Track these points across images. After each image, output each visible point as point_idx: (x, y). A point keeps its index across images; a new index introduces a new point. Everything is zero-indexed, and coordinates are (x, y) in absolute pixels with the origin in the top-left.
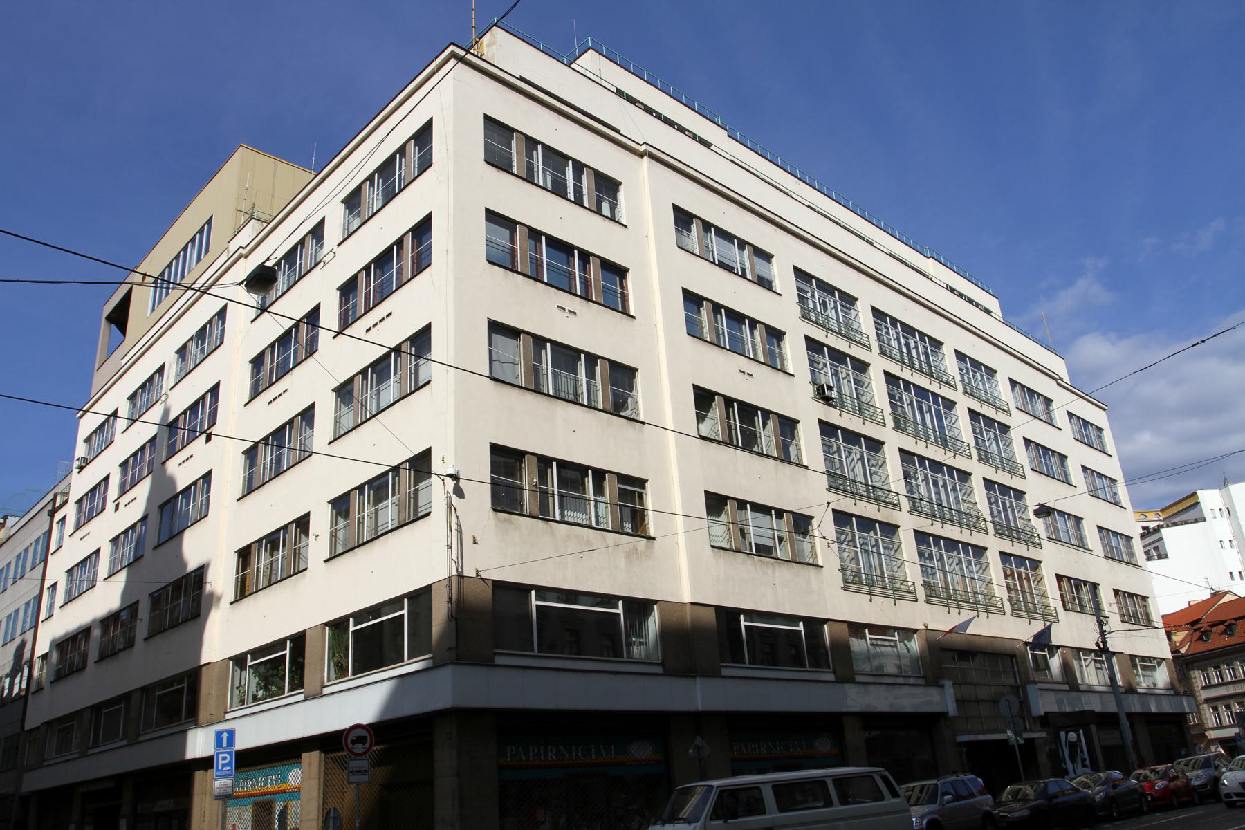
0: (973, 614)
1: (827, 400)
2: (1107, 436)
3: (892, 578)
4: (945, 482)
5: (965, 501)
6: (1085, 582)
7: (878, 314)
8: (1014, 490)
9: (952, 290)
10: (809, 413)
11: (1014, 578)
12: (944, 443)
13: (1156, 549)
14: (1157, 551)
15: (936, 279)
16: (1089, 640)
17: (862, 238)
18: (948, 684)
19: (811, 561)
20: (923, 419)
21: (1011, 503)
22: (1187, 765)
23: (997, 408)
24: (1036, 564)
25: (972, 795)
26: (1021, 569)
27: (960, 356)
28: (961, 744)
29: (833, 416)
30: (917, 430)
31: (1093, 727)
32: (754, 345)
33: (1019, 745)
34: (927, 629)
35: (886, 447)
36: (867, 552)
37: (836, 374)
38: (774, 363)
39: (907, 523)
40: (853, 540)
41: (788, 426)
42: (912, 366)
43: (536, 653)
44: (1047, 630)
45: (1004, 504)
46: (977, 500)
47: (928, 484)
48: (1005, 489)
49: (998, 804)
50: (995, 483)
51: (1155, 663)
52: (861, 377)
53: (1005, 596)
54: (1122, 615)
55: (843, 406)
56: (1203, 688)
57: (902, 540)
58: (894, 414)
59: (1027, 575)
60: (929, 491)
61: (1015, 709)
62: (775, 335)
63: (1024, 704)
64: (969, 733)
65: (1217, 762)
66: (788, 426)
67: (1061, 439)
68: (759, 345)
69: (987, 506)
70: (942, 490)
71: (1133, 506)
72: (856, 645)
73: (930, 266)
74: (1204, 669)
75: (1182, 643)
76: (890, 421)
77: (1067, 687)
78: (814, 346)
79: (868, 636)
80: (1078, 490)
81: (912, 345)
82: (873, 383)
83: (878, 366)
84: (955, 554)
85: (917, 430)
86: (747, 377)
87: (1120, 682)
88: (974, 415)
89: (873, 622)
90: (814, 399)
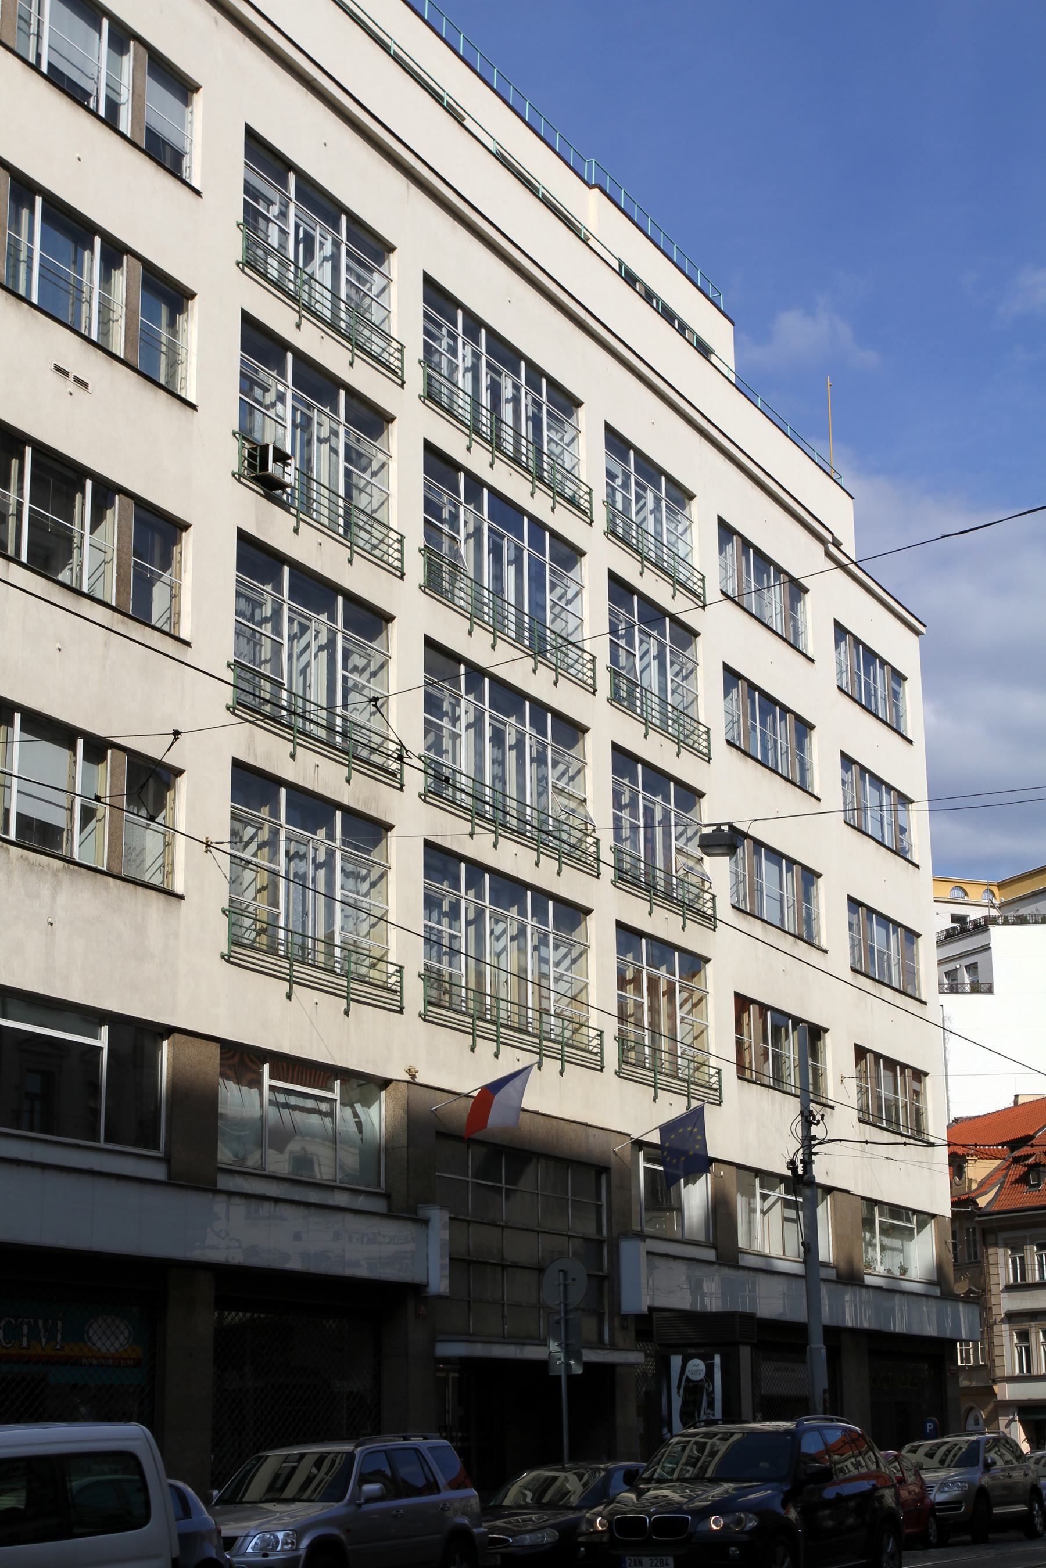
0: (528, 1059)
1: (270, 488)
2: (912, 692)
3: (351, 949)
4: (521, 735)
5: (560, 791)
6: (797, 1021)
7: (437, 297)
8: (679, 783)
9: (630, 279)
10: (217, 509)
11: (638, 990)
12: (537, 646)
13: (972, 968)
14: (967, 974)
15: (597, 245)
16: (776, 1153)
17: (437, 97)
18: (438, 1217)
19: (156, 880)
20: (498, 577)
21: (666, 813)
22: (930, 1455)
24: (695, 963)
25: (432, 1487)
26: (658, 967)
27: (616, 442)
28: (446, 1360)
29: (277, 529)
30: (477, 600)
31: (745, 1352)
32: (105, 307)
33: (571, 1378)
34: (412, 1083)
35: (394, 628)
36: (300, 880)
37: (304, 425)
38: (152, 365)
39: (413, 820)
40: (272, 843)
41: (158, 532)
42: (496, 444)
43: (102, 1144)
44: (694, 1119)
45: (649, 813)
46: (589, 795)
47: (479, 735)
48: (658, 778)
49: (491, 1510)
50: (636, 759)
51: (914, 1224)
52: (365, 446)
53: (611, 1027)
54: (863, 1110)
56: (1009, 1288)
57: (393, 861)
58: (430, 552)
59: (671, 986)
60: (479, 754)
61: (578, 1294)
62: (167, 294)
63: (605, 1283)
64: (469, 1337)
65: (992, 1456)
66: (158, 532)
67: (809, 685)
68: (119, 312)
69: (609, 810)
70: (511, 757)
71: (935, 870)
72: (237, 1100)
73: (591, 207)
74: (1016, 1248)
75: (984, 1185)
76: (416, 567)
78: (260, 342)
79: (267, 1081)
80: (823, 806)
81: (507, 392)
82: (393, 466)
83: (414, 423)
84: (513, 912)
85: (477, 600)
86: (72, 387)
87: (826, 1251)
88: (620, 588)
89: (286, 1049)
90: (237, 476)
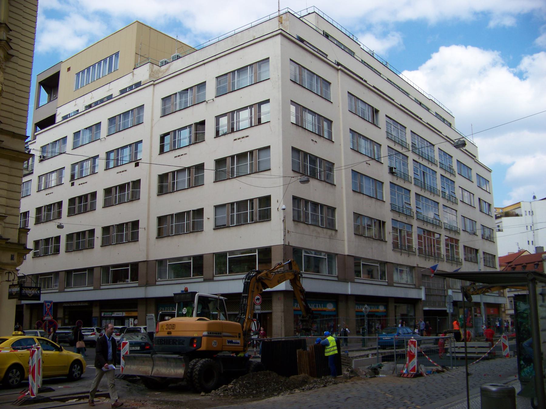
23: (402, 146)
55: (425, 188)
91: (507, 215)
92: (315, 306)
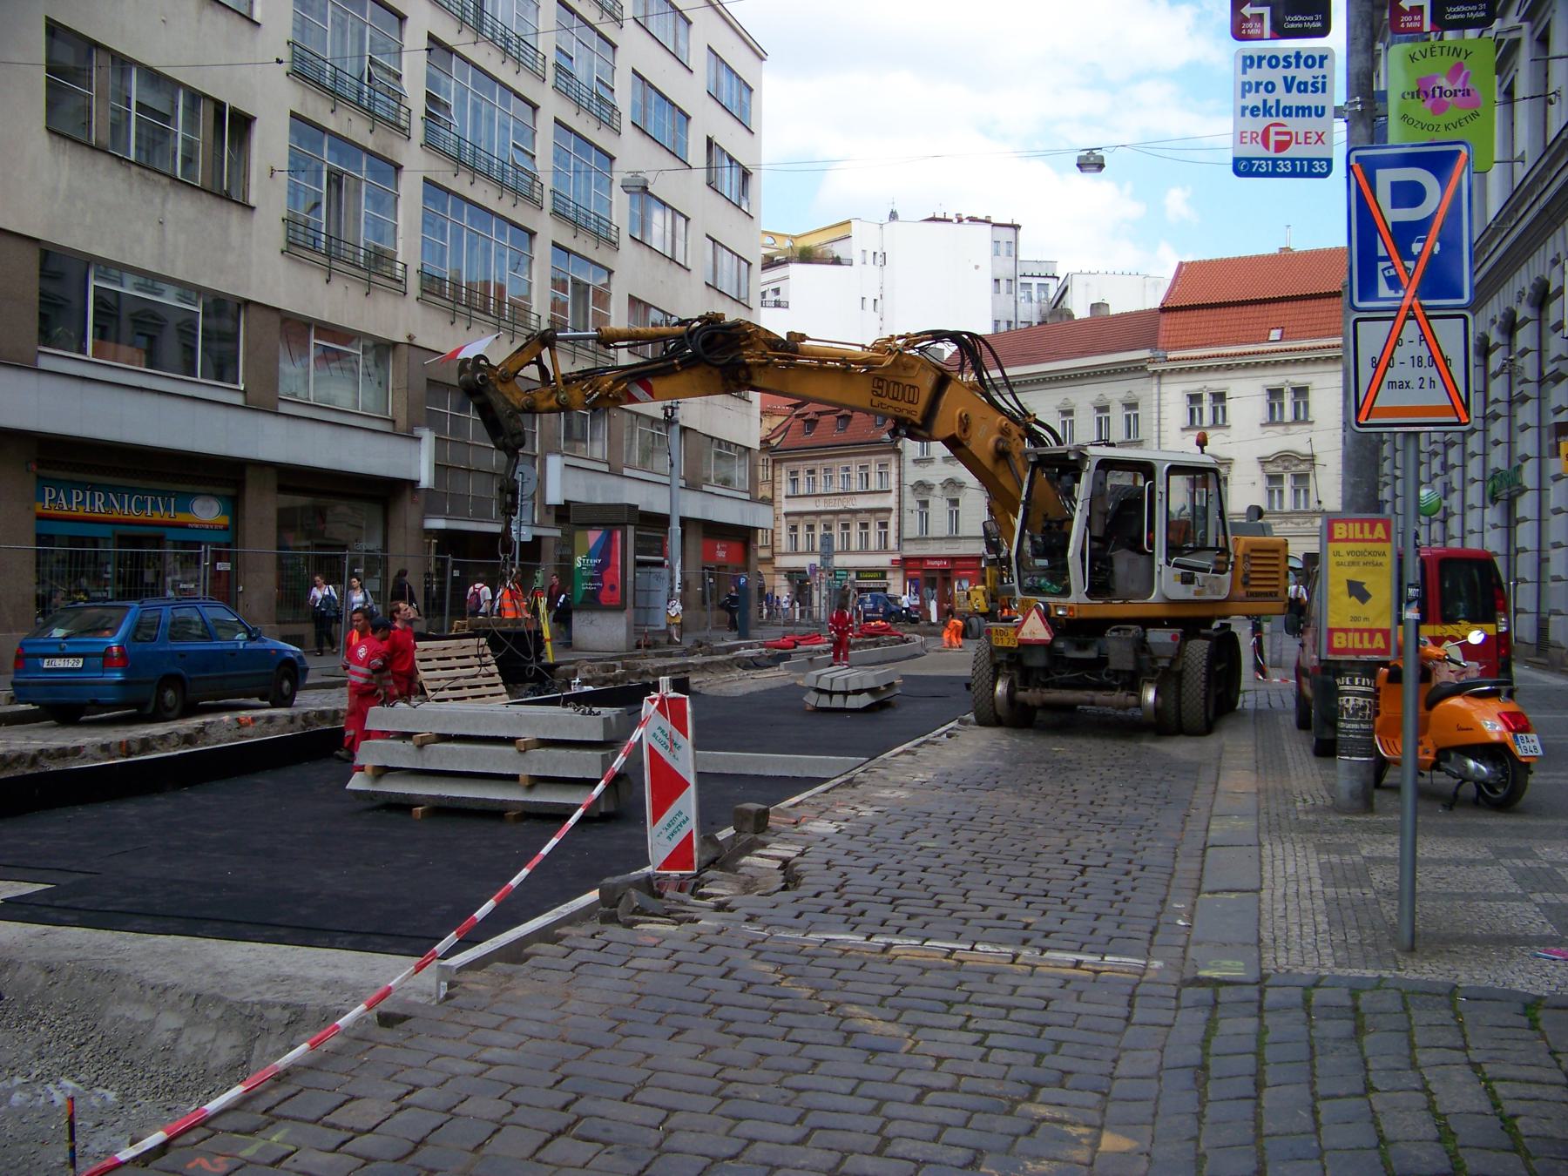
18: (428, 437)
39: (416, 162)
43: (199, 379)
77: (605, 468)
79: (313, 341)
91: (807, 257)
92: (141, 505)
